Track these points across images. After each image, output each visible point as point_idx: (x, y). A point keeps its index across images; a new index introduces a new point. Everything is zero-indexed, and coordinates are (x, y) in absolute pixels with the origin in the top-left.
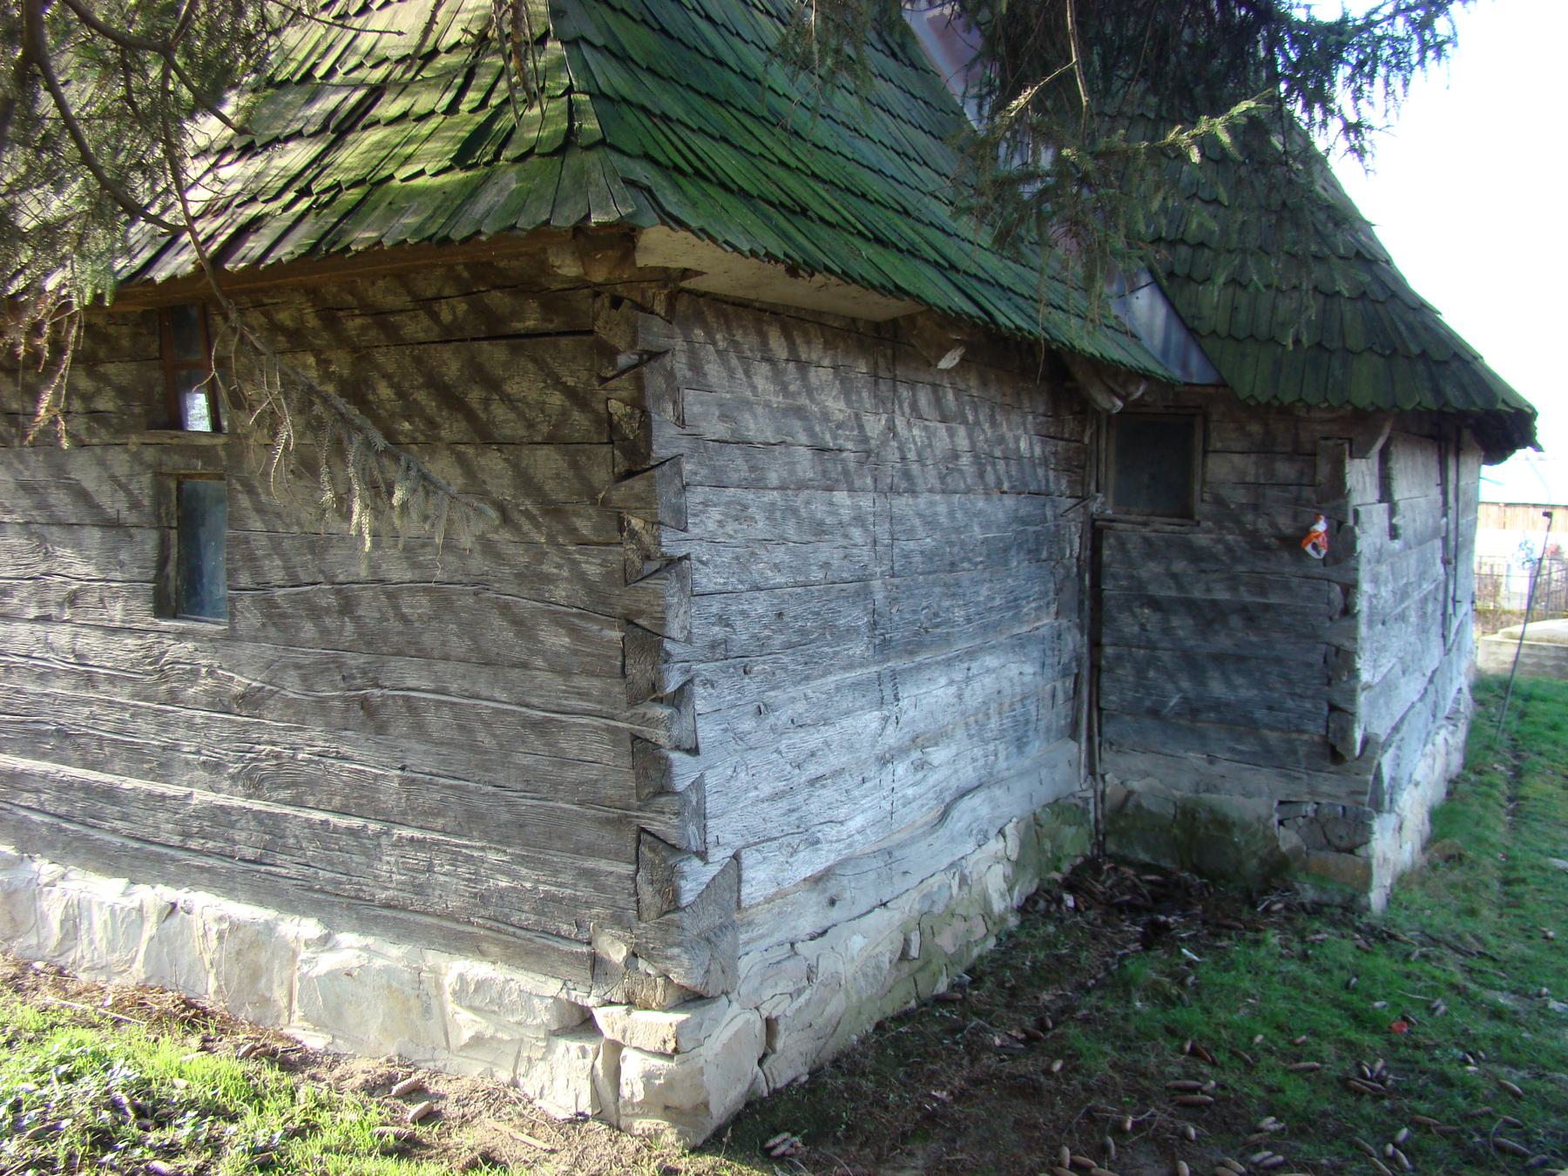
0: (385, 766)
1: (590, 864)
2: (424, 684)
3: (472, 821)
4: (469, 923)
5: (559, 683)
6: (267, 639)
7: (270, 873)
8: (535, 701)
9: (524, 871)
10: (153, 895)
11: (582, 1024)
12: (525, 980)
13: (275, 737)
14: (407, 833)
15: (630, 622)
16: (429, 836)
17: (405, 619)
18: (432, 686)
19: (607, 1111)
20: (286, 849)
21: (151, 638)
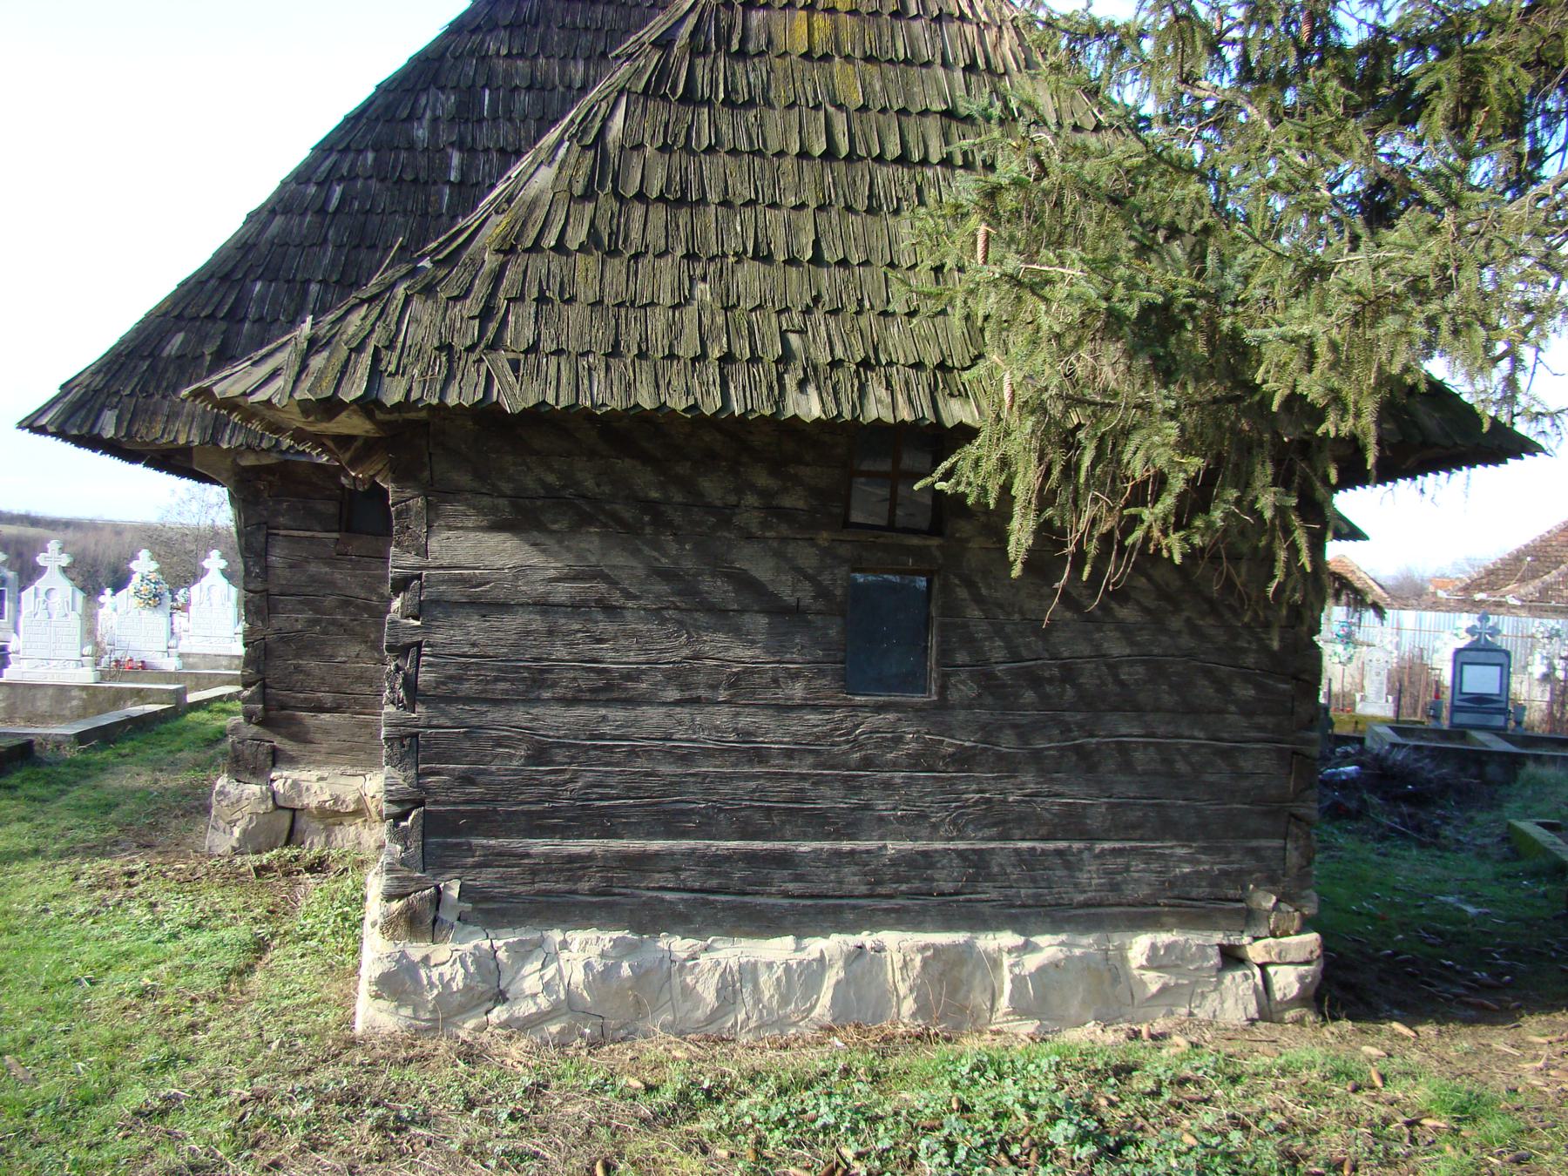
0: (1090, 796)
1: (1254, 843)
2: (1136, 731)
3: (1168, 828)
4: (1158, 905)
5: (1243, 722)
6: (981, 706)
7: (970, 901)
8: (1225, 735)
9: (1203, 857)
10: (832, 945)
11: (1232, 958)
12: (1195, 938)
13: (985, 786)
14: (1107, 845)
15: (1298, 679)
16: (1128, 844)
17: (1122, 684)
18: (1141, 732)
19: (1268, 1010)
20: (990, 877)
21: (838, 715)
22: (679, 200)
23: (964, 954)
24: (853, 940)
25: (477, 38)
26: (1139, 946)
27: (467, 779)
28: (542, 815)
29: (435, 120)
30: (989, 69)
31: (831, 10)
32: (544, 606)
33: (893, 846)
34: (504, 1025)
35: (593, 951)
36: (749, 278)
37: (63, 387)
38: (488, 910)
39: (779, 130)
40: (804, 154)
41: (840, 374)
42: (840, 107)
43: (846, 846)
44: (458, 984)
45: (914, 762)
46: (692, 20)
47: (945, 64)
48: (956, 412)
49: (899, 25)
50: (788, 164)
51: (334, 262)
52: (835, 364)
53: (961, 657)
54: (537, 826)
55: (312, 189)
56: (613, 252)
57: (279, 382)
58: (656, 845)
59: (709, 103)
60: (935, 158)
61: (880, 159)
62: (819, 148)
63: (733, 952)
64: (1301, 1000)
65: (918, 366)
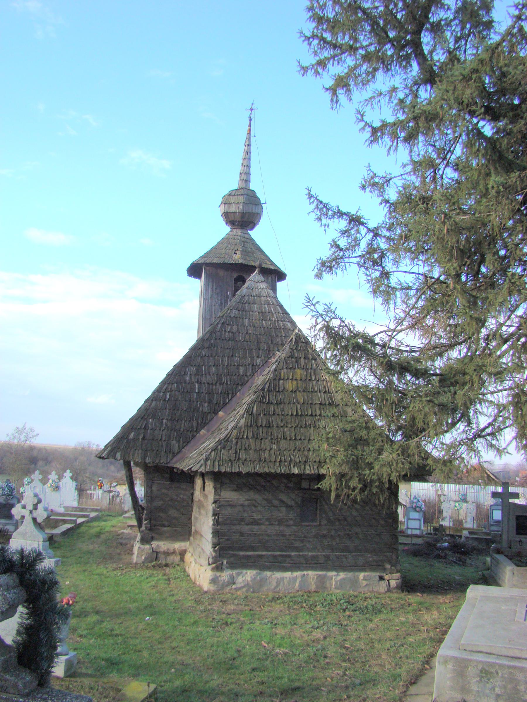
3: (367, 551)
10: (298, 574)
11: (381, 578)
19: (389, 590)
22: (268, 427)
23: (325, 576)
24: (302, 573)
25: (200, 351)
26: (362, 575)
27: (228, 540)
28: (242, 547)
29: (191, 375)
30: (329, 392)
31: (296, 380)
32: (242, 505)
33: (310, 554)
34: (235, 589)
35: (252, 574)
36: (283, 443)
37: (106, 446)
38: (232, 566)
39: (288, 410)
40: (292, 415)
41: (301, 464)
42: (299, 403)
43: (301, 553)
44: (226, 580)
45: (316, 536)
46: (268, 384)
47: (320, 392)
48: (322, 471)
49: (311, 382)
50: (289, 417)
51: (169, 415)
52: (300, 462)
53: (324, 515)
54: (242, 549)
55: (162, 394)
56: (257, 438)
57: (203, 467)
58: (264, 553)
59: (272, 403)
60: (318, 414)
61: (307, 415)
62: (295, 413)
63: (278, 575)
64: (397, 587)
65: (315, 462)
